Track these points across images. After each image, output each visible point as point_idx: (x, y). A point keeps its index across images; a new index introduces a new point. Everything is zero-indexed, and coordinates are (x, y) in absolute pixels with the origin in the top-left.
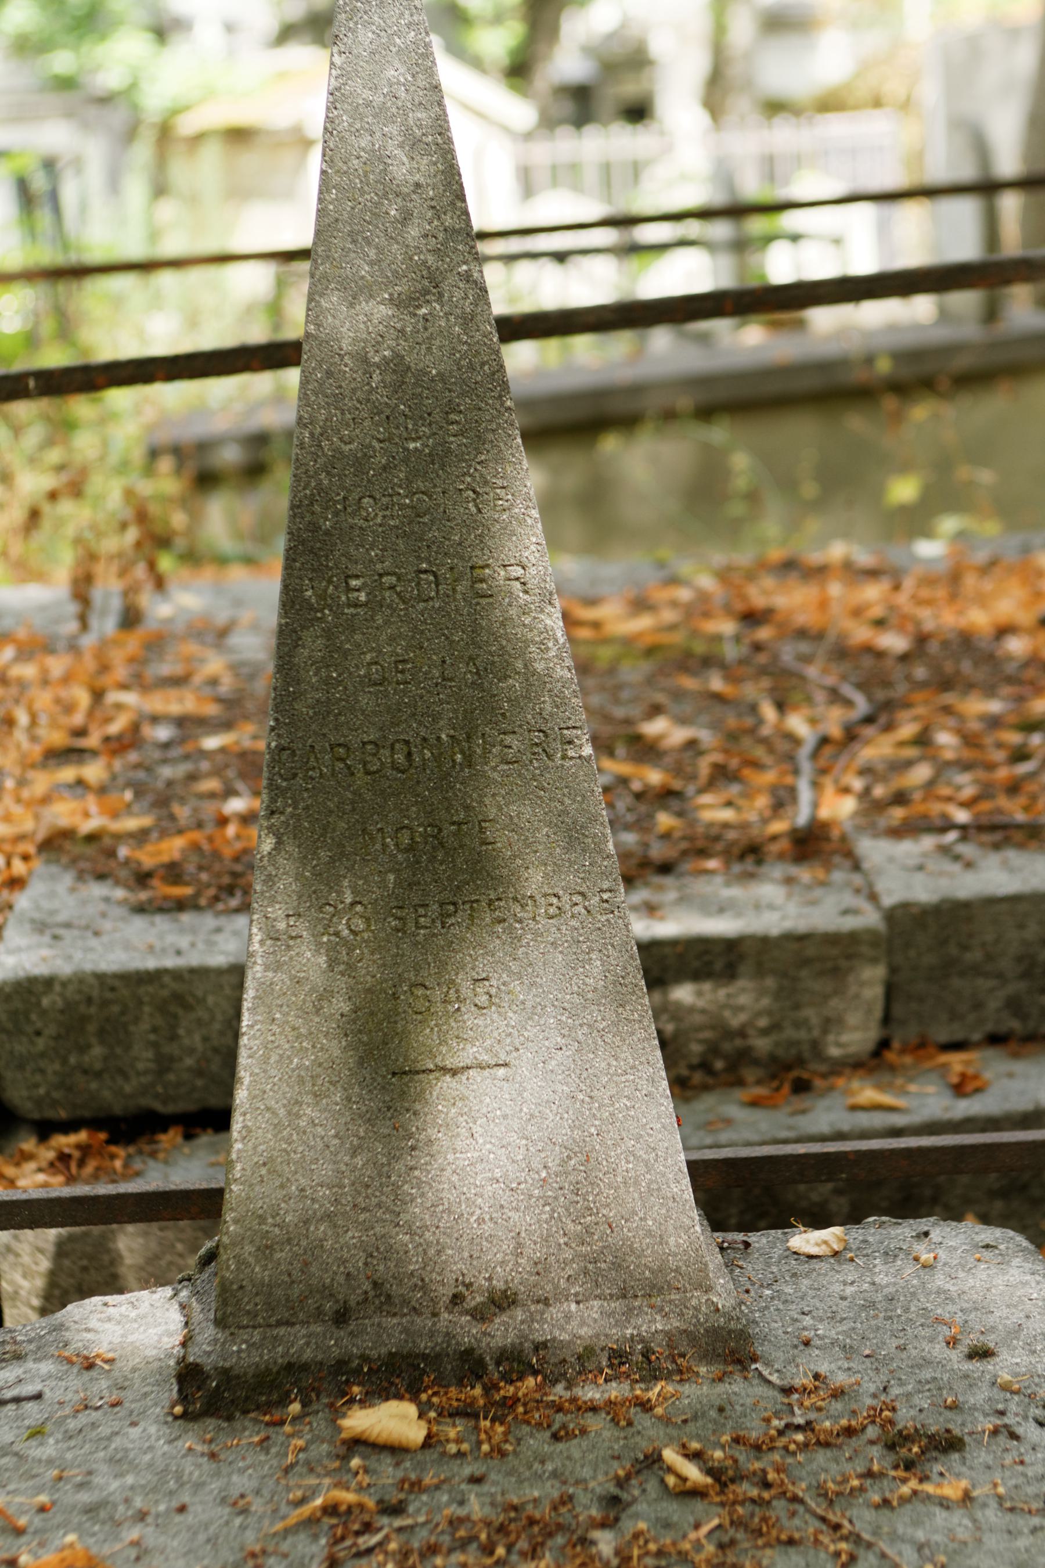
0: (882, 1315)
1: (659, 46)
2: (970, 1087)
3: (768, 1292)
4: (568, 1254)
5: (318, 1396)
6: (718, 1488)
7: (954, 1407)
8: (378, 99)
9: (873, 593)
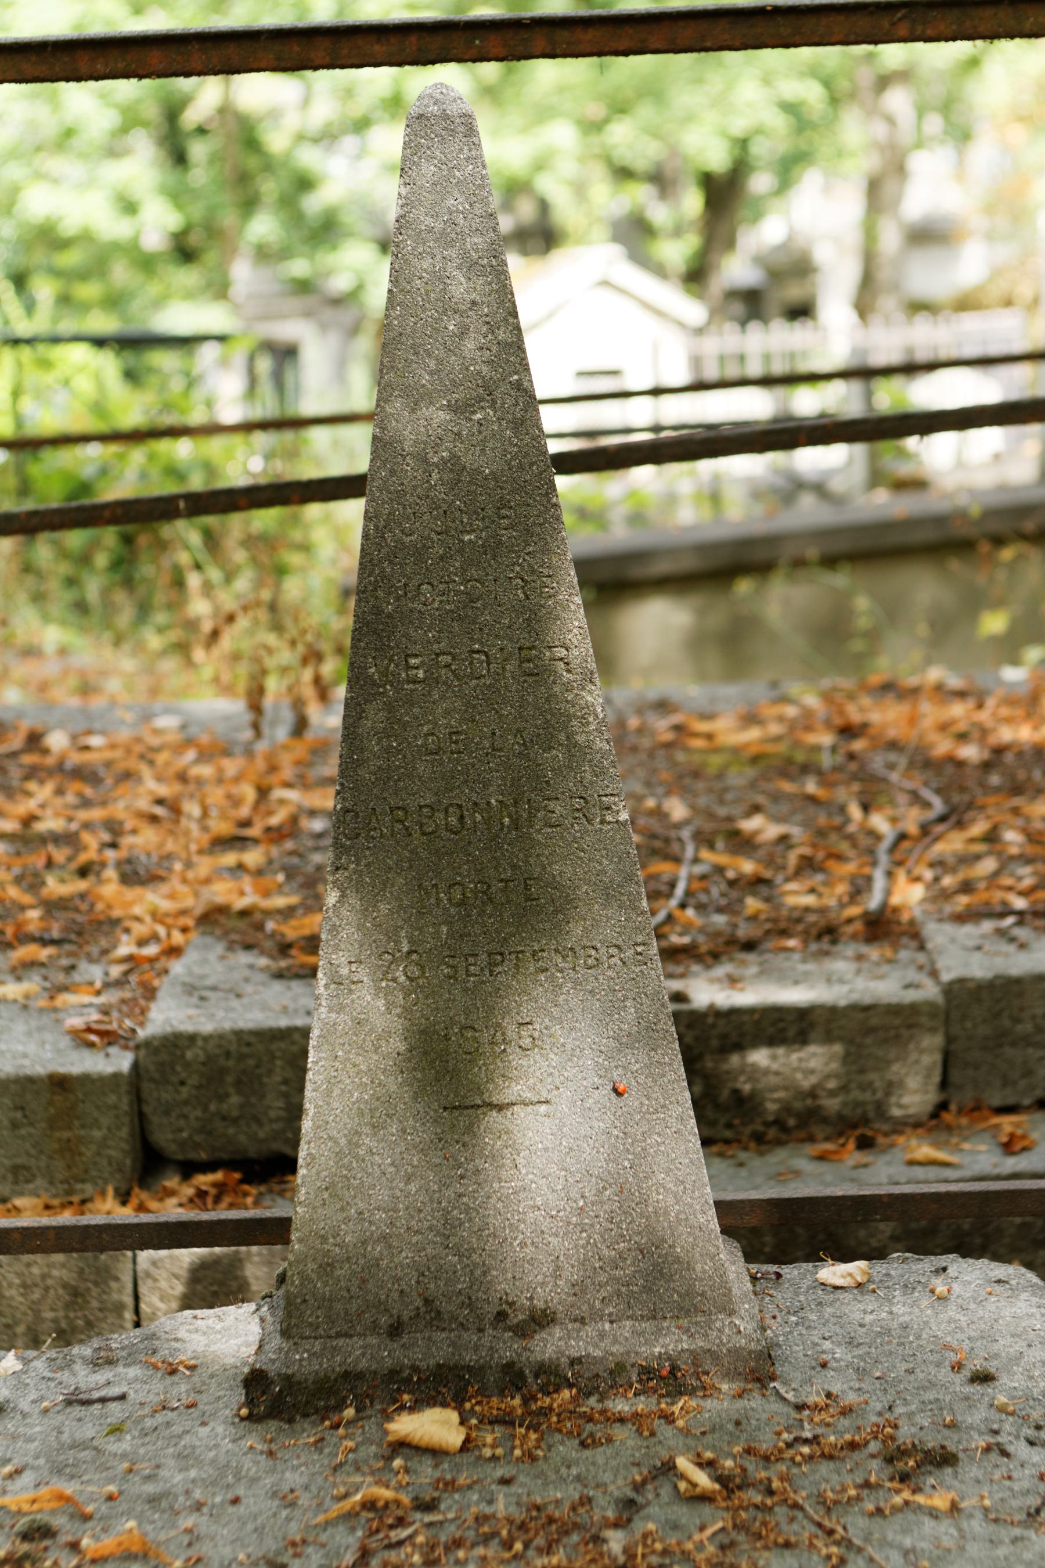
0: (895, 1342)
1: (823, 255)
2: (1018, 1147)
3: (793, 1319)
4: (603, 1278)
5: (372, 1403)
6: (725, 1493)
7: (952, 1426)
8: (439, 226)
9: (958, 710)
